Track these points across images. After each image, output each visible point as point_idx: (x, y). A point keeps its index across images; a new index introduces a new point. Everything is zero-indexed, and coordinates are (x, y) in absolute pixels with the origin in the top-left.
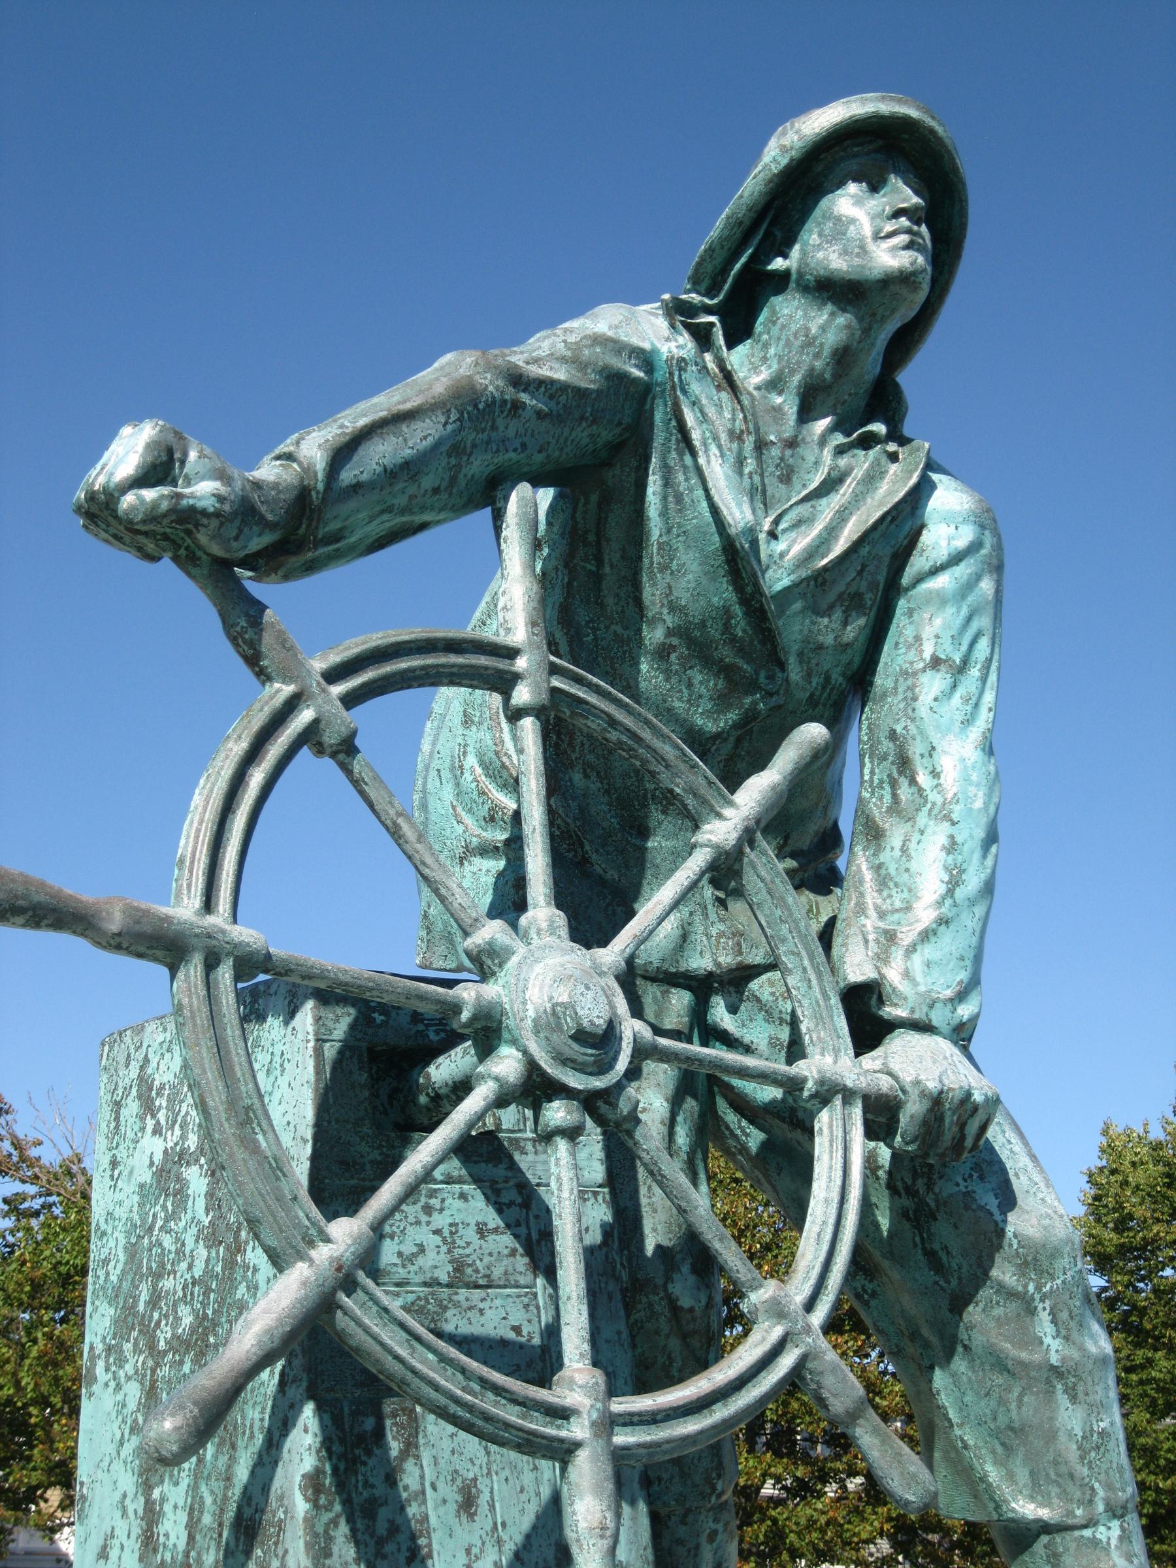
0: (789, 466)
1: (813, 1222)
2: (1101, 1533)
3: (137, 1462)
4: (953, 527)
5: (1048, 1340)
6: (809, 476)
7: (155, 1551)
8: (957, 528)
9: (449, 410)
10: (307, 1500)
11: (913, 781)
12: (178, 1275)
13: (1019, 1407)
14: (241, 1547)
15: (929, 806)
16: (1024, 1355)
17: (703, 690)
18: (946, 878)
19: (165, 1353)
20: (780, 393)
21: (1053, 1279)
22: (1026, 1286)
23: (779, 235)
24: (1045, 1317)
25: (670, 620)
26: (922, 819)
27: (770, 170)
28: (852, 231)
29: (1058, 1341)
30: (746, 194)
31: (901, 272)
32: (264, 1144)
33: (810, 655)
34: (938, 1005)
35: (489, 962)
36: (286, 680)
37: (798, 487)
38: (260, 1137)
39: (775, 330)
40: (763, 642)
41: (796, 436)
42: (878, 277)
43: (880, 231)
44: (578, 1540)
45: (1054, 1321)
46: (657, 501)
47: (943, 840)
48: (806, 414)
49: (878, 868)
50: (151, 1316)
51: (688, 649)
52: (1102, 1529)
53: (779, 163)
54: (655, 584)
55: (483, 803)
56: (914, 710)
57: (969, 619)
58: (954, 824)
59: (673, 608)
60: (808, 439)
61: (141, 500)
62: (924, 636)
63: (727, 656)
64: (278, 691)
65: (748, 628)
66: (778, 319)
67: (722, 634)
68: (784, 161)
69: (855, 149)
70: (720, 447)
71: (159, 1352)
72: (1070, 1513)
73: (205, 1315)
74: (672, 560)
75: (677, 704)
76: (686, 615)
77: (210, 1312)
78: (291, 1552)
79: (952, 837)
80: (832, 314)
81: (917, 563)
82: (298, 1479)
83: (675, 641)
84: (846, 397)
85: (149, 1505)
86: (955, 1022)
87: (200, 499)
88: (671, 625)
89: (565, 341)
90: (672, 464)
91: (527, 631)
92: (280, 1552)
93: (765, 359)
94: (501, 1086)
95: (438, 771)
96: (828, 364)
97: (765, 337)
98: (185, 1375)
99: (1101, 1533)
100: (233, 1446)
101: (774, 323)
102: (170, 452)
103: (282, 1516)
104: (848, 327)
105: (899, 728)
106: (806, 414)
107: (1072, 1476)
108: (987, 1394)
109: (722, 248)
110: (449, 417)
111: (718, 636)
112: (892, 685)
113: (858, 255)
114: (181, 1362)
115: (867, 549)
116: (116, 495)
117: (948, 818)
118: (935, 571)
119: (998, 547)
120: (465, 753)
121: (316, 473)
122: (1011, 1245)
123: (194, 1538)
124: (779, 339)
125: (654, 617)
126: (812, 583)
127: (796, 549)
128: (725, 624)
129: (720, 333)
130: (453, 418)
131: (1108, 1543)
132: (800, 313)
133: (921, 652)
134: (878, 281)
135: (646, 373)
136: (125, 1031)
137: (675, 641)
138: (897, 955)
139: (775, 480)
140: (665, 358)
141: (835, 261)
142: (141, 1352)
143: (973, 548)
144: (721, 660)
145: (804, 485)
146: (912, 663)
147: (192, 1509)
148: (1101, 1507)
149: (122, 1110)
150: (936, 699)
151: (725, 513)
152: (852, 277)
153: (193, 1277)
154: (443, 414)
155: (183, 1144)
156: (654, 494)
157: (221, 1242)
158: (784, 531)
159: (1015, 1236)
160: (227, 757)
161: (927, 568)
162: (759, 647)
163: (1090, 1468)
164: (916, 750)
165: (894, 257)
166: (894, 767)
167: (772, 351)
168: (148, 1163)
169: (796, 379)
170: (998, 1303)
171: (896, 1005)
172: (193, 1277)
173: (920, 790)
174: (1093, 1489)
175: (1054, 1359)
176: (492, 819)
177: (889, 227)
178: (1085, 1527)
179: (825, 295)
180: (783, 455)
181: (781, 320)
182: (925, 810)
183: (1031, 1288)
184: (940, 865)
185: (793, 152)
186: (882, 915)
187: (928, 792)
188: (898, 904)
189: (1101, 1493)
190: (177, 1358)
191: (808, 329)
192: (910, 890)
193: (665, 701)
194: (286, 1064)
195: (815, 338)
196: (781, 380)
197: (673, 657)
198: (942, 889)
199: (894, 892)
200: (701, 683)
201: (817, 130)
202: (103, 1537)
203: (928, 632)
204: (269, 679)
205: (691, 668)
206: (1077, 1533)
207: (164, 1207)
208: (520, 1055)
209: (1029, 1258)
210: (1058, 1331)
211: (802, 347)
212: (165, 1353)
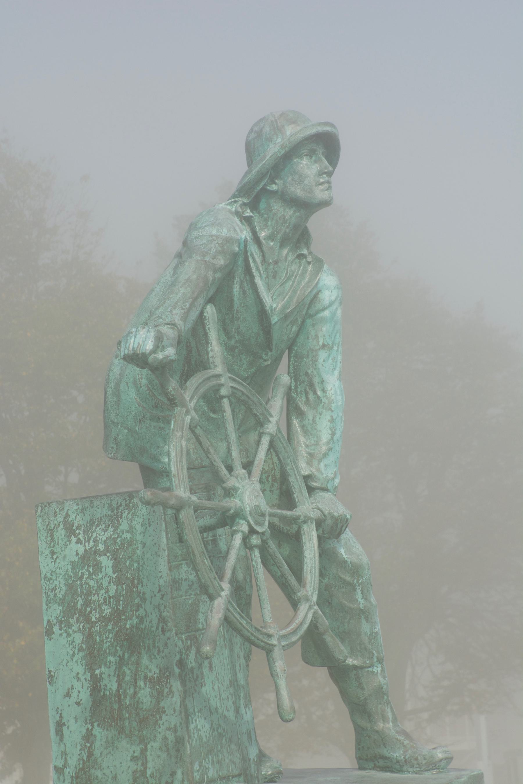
1: (307, 566)
2: (375, 669)
3: (84, 661)
5: (360, 600)
7: (100, 691)
10: (179, 668)
11: (315, 393)
12: (100, 595)
13: (348, 624)
14: (148, 686)
15: (323, 404)
16: (352, 606)
17: (245, 362)
18: (330, 433)
19: (96, 623)
20: (272, 241)
21: (362, 578)
22: (353, 581)
24: (359, 592)
26: (320, 409)
28: (306, 182)
29: (363, 600)
32: (207, 563)
34: (330, 481)
35: (232, 492)
38: (206, 561)
44: (277, 675)
45: (362, 593)
47: (329, 418)
48: (282, 246)
49: (303, 427)
50: (86, 610)
52: (375, 668)
55: (152, 400)
56: (316, 365)
57: (334, 327)
58: (332, 411)
62: (320, 336)
66: (272, 210)
71: (93, 622)
72: (365, 662)
73: (118, 609)
75: (235, 367)
77: (121, 608)
78: (174, 686)
79: (332, 417)
80: (295, 211)
81: (318, 306)
82: (175, 662)
85: (94, 677)
86: (334, 487)
92: (168, 686)
93: (266, 226)
94: (243, 534)
95: (127, 383)
97: (266, 216)
98: (109, 630)
99: (375, 669)
100: (139, 653)
101: (271, 211)
103: (168, 675)
105: (310, 372)
107: (366, 649)
108: (337, 620)
112: (306, 354)
113: (309, 192)
114: (107, 626)
117: (330, 409)
118: (324, 309)
120: (141, 378)
122: (349, 566)
123: (121, 685)
124: (273, 219)
131: (377, 673)
132: (282, 209)
133: (319, 342)
136: (52, 502)
137: (238, 345)
138: (315, 463)
140: (243, 240)
142: (81, 622)
145: (280, 278)
146: (315, 346)
147: (119, 676)
148: (375, 660)
149: (54, 533)
150: (324, 361)
153: (109, 595)
155: (96, 548)
156: (236, 291)
157: (124, 584)
159: (351, 563)
160: (177, 438)
161: (321, 308)
163: (372, 646)
164: (316, 381)
166: (307, 387)
167: (269, 223)
168: (75, 553)
169: (280, 236)
170: (343, 587)
171: (316, 482)
172: (109, 595)
173: (318, 397)
174: (373, 653)
175: (362, 607)
176: (156, 406)
178: (370, 667)
182: (321, 406)
183: (355, 581)
184: (328, 427)
186: (307, 446)
187: (322, 398)
188: (313, 442)
189: (376, 654)
190: (104, 624)
192: (317, 437)
193: (232, 366)
194: (151, 523)
197: (236, 351)
198: (329, 437)
199: (310, 437)
200: (244, 359)
202: (67, 689)
206: (366, 670)
207: (88, 570)
208: (246, 523)
209: (355, 571)
210: (363, 597)
212: (96, 623)
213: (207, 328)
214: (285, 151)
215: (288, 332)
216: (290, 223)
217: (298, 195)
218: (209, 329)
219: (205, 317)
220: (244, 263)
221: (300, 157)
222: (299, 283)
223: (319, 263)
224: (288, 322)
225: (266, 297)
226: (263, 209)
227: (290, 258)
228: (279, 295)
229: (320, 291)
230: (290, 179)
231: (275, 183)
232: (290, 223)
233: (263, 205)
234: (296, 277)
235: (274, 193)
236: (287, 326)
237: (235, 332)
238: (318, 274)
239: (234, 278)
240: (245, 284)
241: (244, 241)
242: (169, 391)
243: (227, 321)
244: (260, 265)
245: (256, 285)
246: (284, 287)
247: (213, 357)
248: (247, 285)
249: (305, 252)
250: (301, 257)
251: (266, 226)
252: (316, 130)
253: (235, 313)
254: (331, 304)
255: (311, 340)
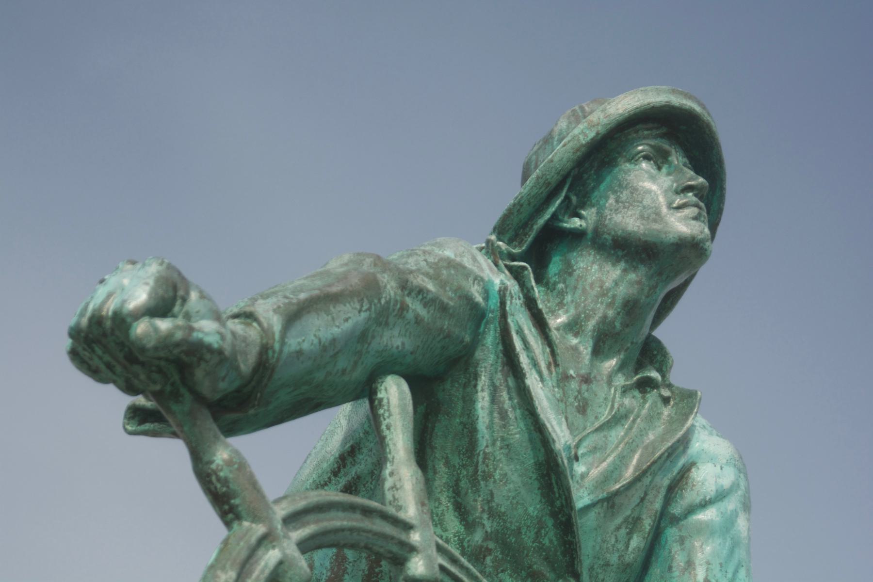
0: (584, 399)
4: (718, 467)
6: (600, 410)
8: (721, 468)
9: (362, 299)
20: (576, 335)
23: (574, 199)
25: (489, 525)
27: (578, 140)
30: (556, 159)
31: (693, 238)
33: (599, 571)
36: (256, 518)
37: (592, 418)
39: (571, 281)
40: (564, 554)
41: (590, 373)
42: (672, 240)
43: (673, 202)
46: (485, 415)
51: (502, 553)
53: (586, 135)
54: (478, 491)
57: (732, 552)
59: (493, 514)
60: (598, 378)
61: (156, 330)
63: (535, 563)
64: (249, 530)
65: (554, 539)
66: (575, 271)
67: (533, 542)
68: (591, 135)
69: (646, 132)
70: (540, 373)
74: (495, 469)
76: (505, 521)
80: (625, 271)
81: (690, 497)
83: (491, 545)
84: (629, 345)
87: (207, 334)
88: (489, 530)
89: (425, 260)
90: (498, 384)
91: (418, 509)
96: (618, 314)
97: (561, 286)
101: (570, 274)
102: (175, 288)
104: (639, 283)
106: (598, 352)
109: (529, 204)
110: (362, 306)
111: (529, 544)
113: (655, 221)
115: (649, 479)
116: (129, 320)
118: (704, 504)
119: (748, 490)
121: (273, 334)
125: (474, 520)
126: (605, 504)
127: (595, 473)
128: (536, 533)
129: (532, 275)
130: (364, 308)
132: (596, 267)
134: (672, 244)
135: (484, 299)
137: (491, 545)
139: (574, 410)
140: (497, 288)
141: (628, 221)
143: (734, 487)
144: (530, 567)
151: (550, 429)
152: (649, 239)
154: (359, 301)
156: (482, 408)
158: (583, 455)
161: (698, 501)
162: (561, 557)
165: (687, 225)
169: (591, 324)
177: (678, 201)
179: (620, 253)
180: (580, 389)
181: (577, 272)
185: (600, 128)
191: (602, 283)
195: (609, 290)
196: (576, 324)
197: (488, 560)
201: (621, 111)
203: (700, 558)
204: (238, 517)
205: (502, 571)
211: (597, 297)
213: (384, 427)
214: (598, 134)
215: (620, 546)
216: (614, 296)
217: (630, 228)
218: (388, 428)
219: (381, 400)
220: (500, 347)
221: (633, 159)
222: (642, 433)
223: (687, 400)
224: (619, 520)
225: (554, 423)
226: (555, 275)
227: (620, 380)
228: (594, 450)
229: (693, 464)
230: (611, 201)
231: (580, 217)
232: (614, 296)
233: (554, 267)
234: (634, 421)
235: (578, 236)
236: (618, 528)
237: (483, 511)
238: (687, 419)
239: (476, 377)
240: (505, 395)
241: (500, 291)
242: (213, 466)
243: (463, 484)
244: (545, 372)
245: (532, 399)
246: (605, 437)
247: (394, 487)
248: (510, 399)
249: (654, 374)
250: (645, 385)
251: (561, 305)
252: (666, 99)
253: (481, 459)
254: (721, 496)
255: (676, 574)
